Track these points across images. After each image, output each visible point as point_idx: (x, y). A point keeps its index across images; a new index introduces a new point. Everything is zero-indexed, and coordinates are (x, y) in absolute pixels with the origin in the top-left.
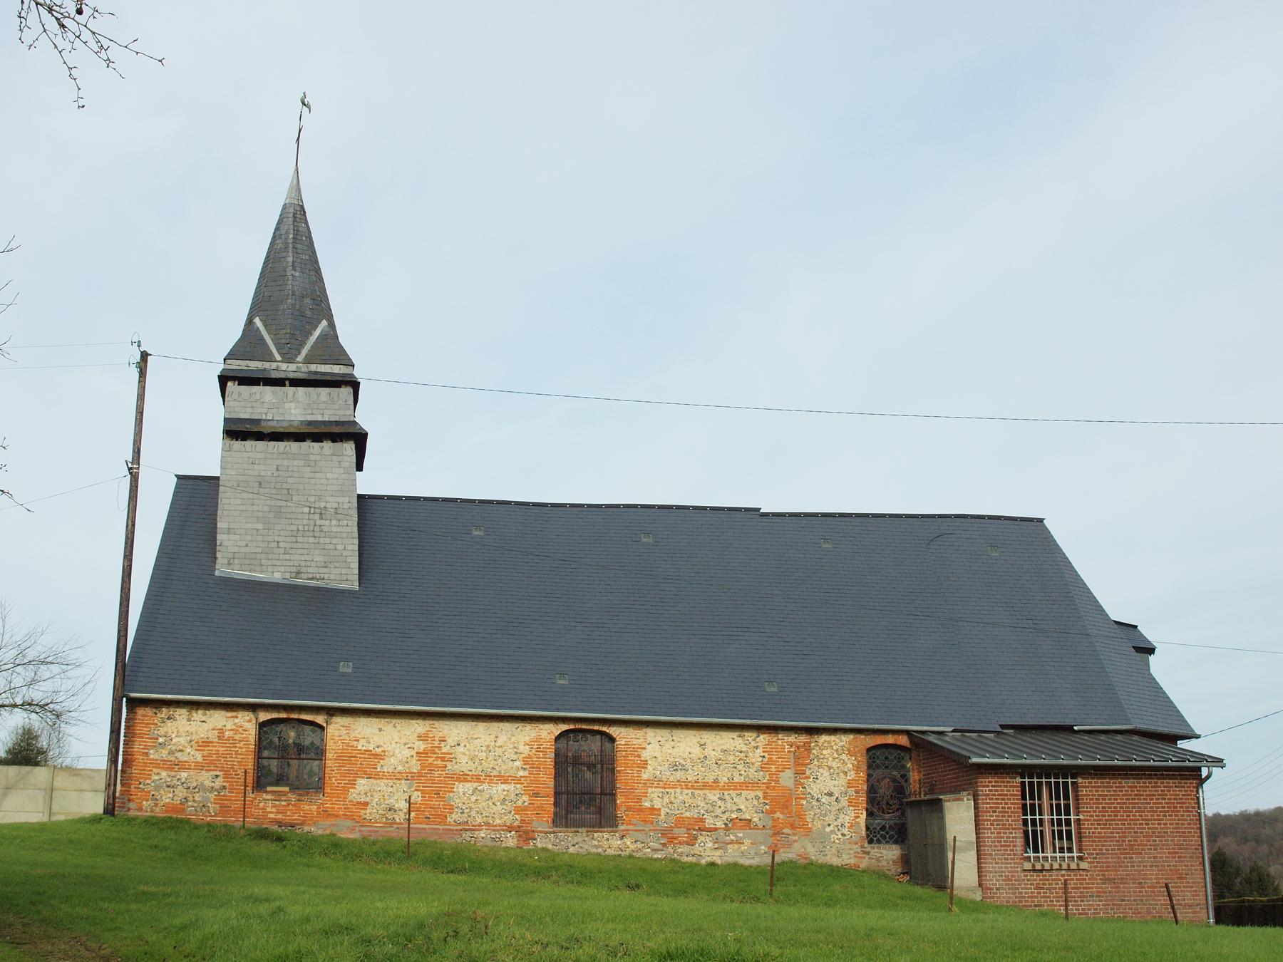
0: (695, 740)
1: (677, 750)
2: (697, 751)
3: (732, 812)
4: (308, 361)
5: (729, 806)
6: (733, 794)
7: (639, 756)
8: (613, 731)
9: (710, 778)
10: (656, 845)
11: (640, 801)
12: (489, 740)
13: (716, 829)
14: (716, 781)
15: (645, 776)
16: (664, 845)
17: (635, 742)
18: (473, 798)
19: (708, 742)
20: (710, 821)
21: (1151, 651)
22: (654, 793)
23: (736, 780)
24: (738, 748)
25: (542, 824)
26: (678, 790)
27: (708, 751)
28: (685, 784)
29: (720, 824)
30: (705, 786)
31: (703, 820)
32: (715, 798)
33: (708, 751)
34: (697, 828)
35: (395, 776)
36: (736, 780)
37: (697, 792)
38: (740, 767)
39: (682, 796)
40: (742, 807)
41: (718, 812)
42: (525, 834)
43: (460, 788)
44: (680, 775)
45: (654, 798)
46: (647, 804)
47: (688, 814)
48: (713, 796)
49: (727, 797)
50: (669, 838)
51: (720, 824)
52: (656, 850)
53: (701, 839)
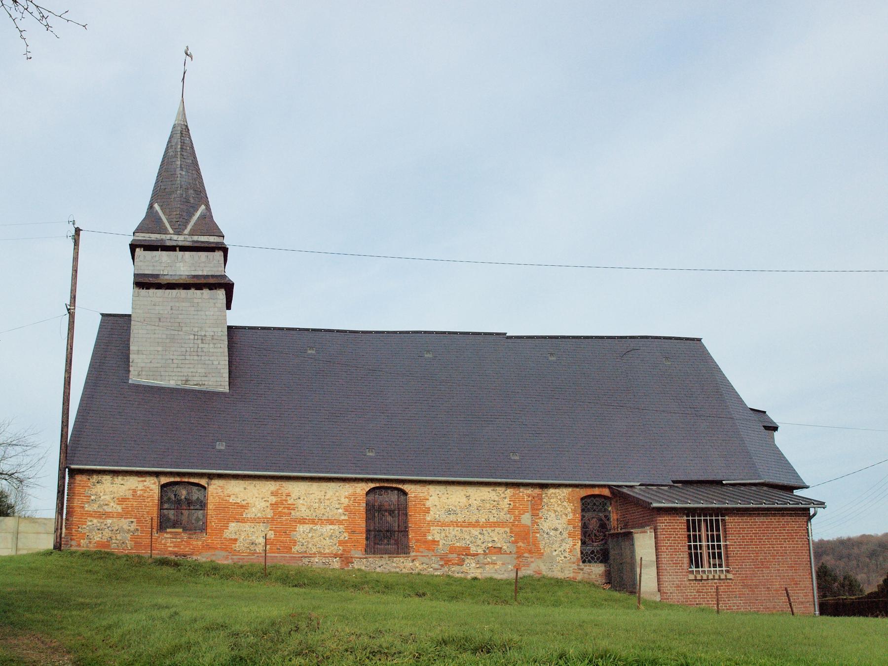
0: (463, 493)
3: (489, 542)
5: (486, 538)
6: (489, 530)
7: (424, 505)
8: (406, 487)
9: (473, 519)
10: (436, 566)
11: (425, 535)
13: (477, 555)
14: (477, 522)
15: (428, 519)
16: (442, 566)
17: (421, 495)
18: (310, 535)
20: (473, 549)
25: (357, 553)
26: (451, 528)
28: (456, 524)
29: (480, 551)
31: (468, 548)
34: (464, 553)
35: (255, 521)
37: (464, 529)
38: (494, 511)
39: (454, 531)
40: (496, 539)
41: (479, 542)
43: (301, 528)
44: (452, 518)
45: (435, 534)
46: (430, 538)
47: (458, 544)
48: (475, 532)
49: (485, 532)
51: (480, 551)
53: (467, 561)
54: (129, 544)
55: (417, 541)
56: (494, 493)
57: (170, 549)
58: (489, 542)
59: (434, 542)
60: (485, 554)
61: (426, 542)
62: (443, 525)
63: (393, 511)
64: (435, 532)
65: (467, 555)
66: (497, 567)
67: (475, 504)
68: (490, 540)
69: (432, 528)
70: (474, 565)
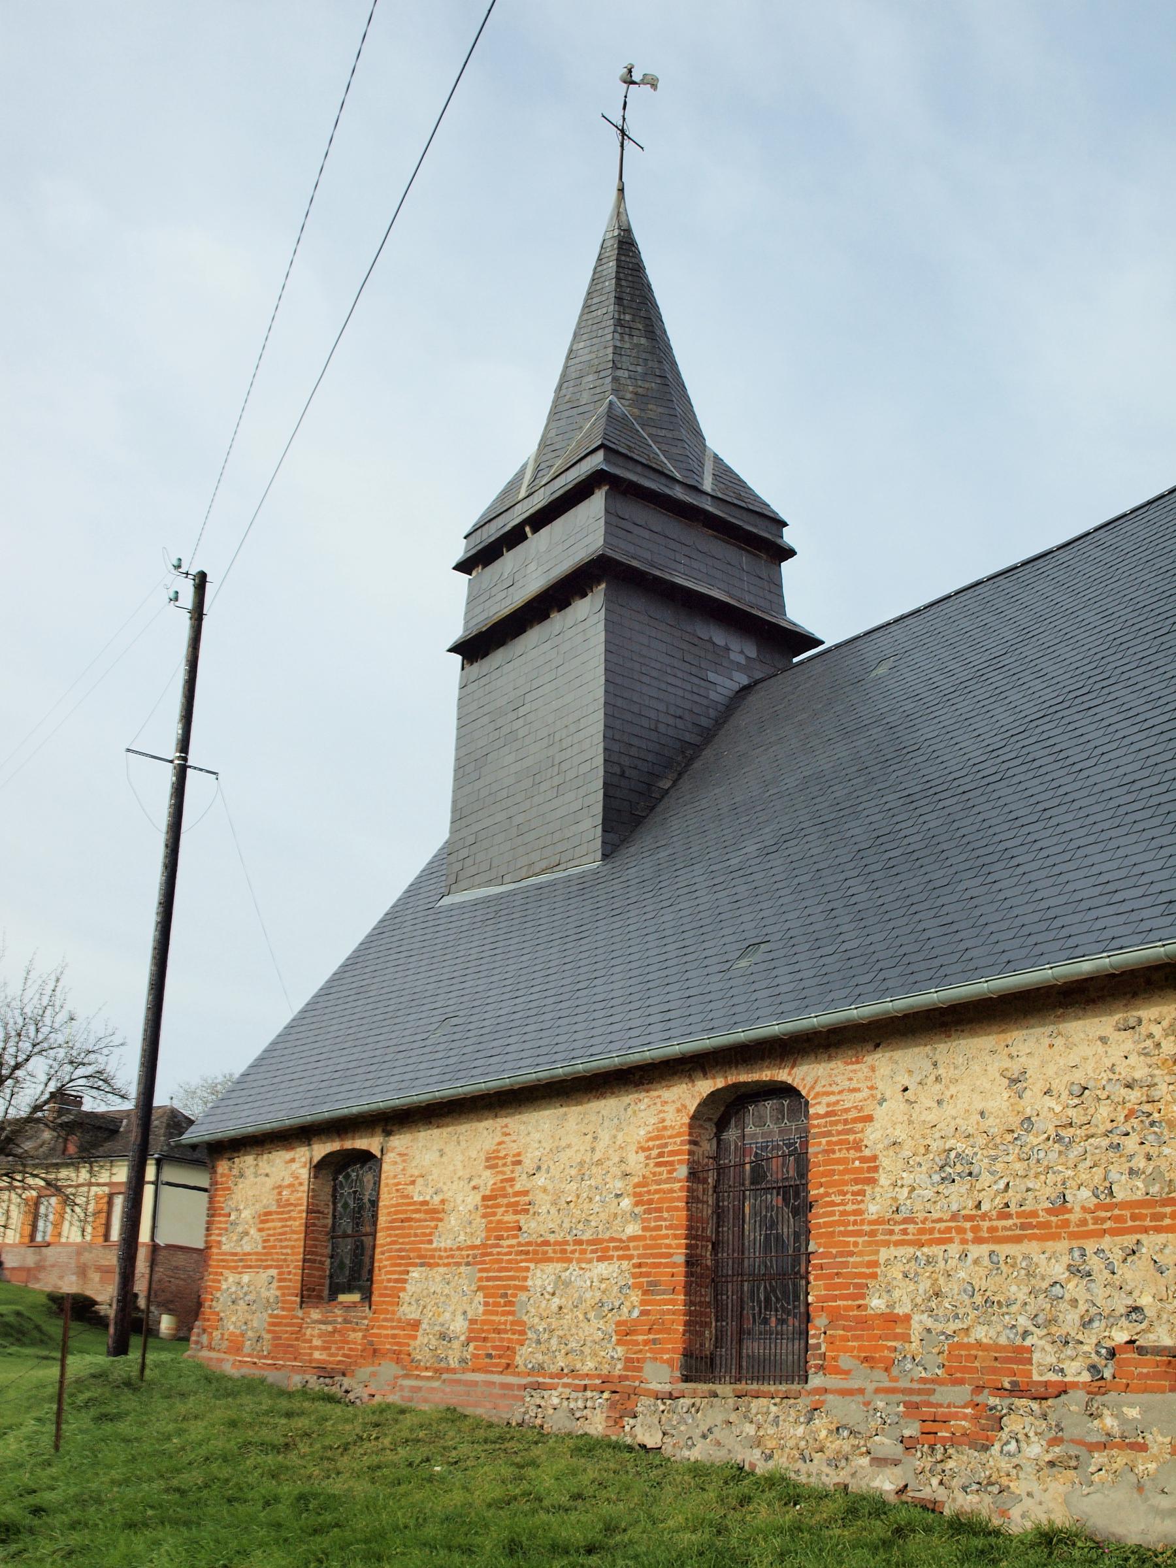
0: (997, 1064)
1: (949, 1110)
2: (999, 1101)
3: (1111, 1319)
4: (650, 435)
5: (1100, 1293)
6: (1113, 1246)
7: (858, 1146)
8: (803, 1075)
9: (1040, 1194)
10: (886, 1444)
11: (860, 1293)
12: (578, 1148)
13: (1063, 1390)
14: (1061, 1205)
15: (873, 1209)
16: (909, 1445)
17: (849, 1100)
18: (556, 1302)
19: (1032, 1065)
20: (1045, 1362)
21: (785, 524)
22: (894, 1259)
23: (1120, 1195)
24: (1123, 1071)
25: (660, 1375)
26: (954, 1249)
27: (1033, 1102)
28: (971, 1226)
29: (1075, 1371)
30: (1032, 1227)
31: (1022, 1355)
32: (1058, 1270)
33: (1033, 1102)
34: (1006, 1382)
35: (451, 1259)
36: (1120, 1195)
37: (1004, 1250)
38: (1131, 1144)
39: (965, 1267)
40: (1145, 1301)
41: (1070, 1320)
42: (622, 1395)
43: (541, 1277)
44: (958, 1197)
45: (895, 1288)
46: (876, 1304)
47: (981, 1333)
48: (1052, 1261)
49: (1095, 1263)
50: (931, 1433)
51: (1075, 1371)
52: (880, 1462)
53: (1013, 1424)
54: (883, 1307)
55: (835, 1317)
56: (1125, 1043)
57: (317, 1355)
58: (1111, 1319)
59: (891, 1319)
60: (1098, 1386)
61: (863, 1322)
62: (925, 1234)
63: (359, 1212)
64: (896, 1272)
65: (1017, 1391)
66: (1146, 1466)
67: (1050, 1112)
68: (1121, 1303)
69: (884, 1254)
70: (1034, 1449)
